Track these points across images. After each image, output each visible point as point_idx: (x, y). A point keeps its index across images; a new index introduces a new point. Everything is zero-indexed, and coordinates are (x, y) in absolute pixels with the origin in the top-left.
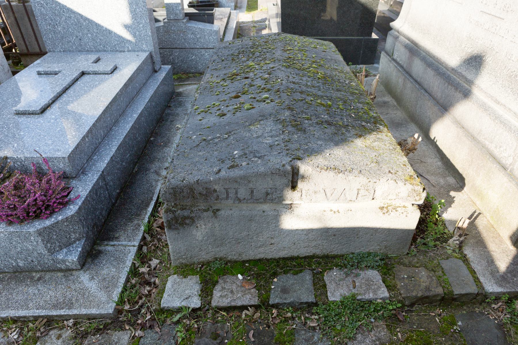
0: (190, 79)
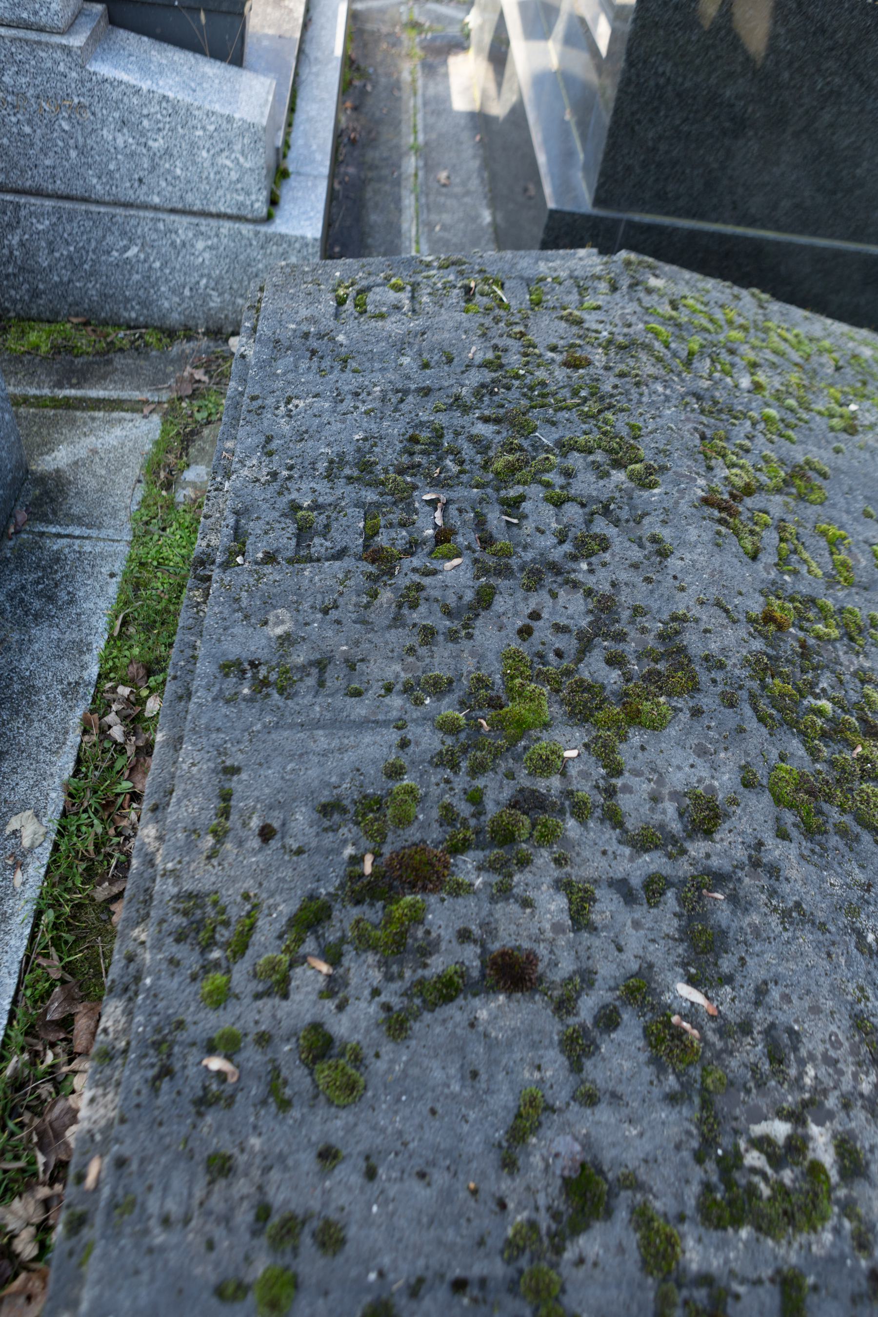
0: (119, 361)
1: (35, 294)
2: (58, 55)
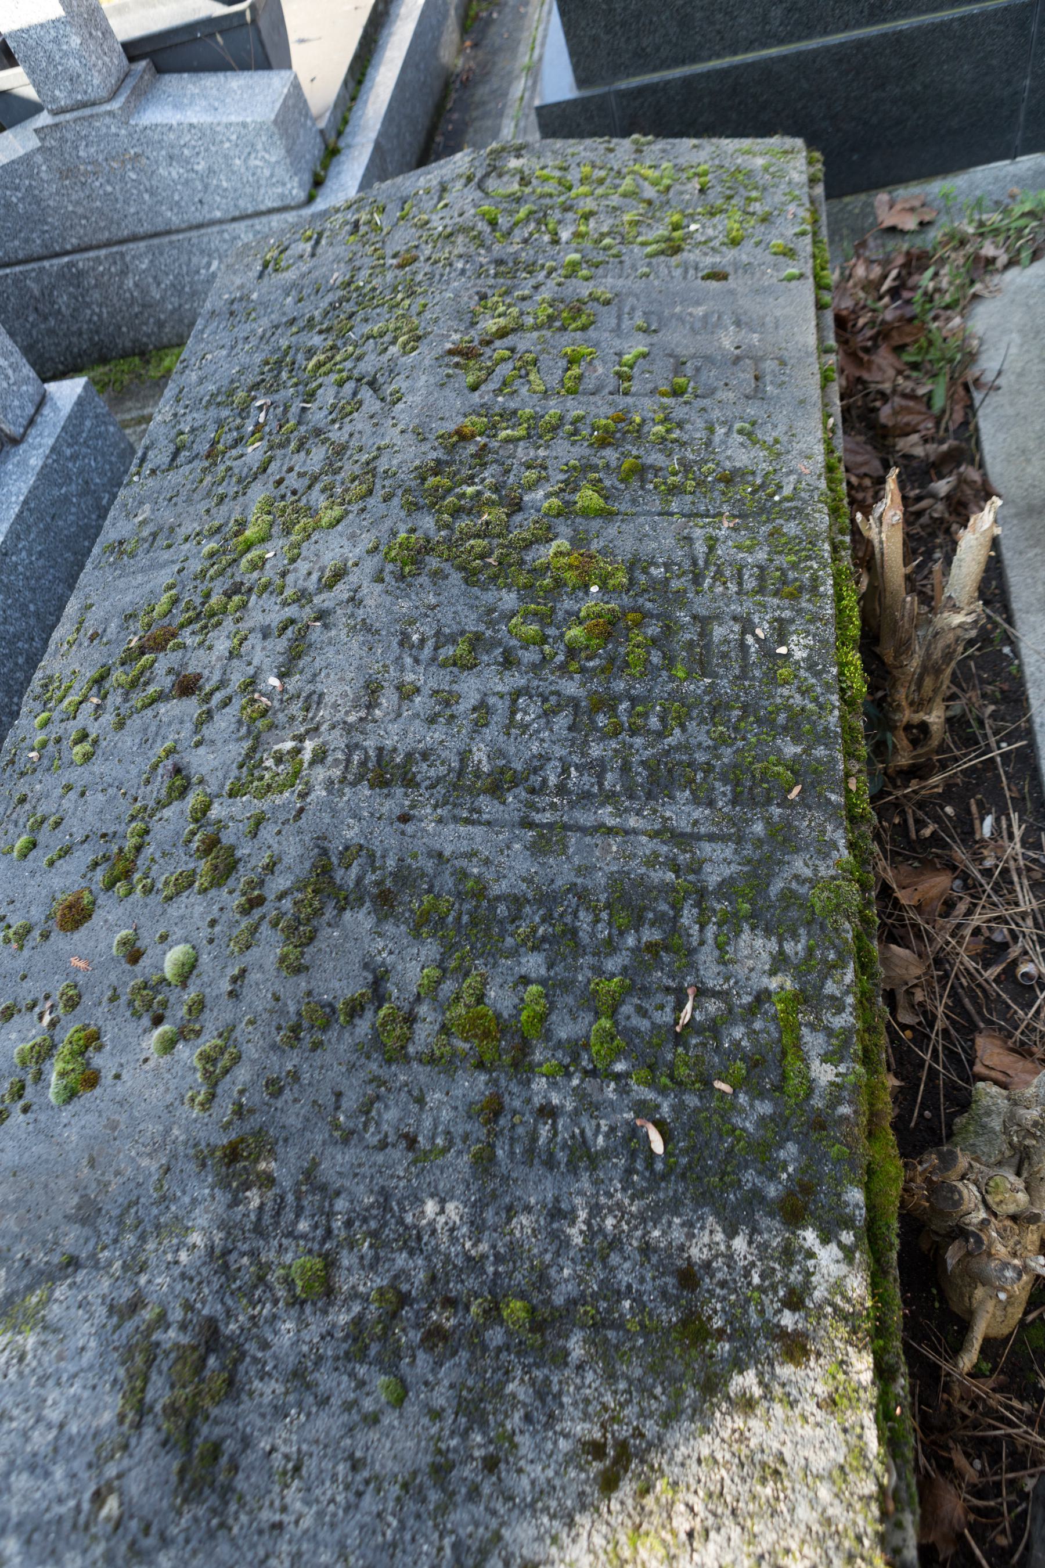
1: (161, 324)
2: (108, 120)
